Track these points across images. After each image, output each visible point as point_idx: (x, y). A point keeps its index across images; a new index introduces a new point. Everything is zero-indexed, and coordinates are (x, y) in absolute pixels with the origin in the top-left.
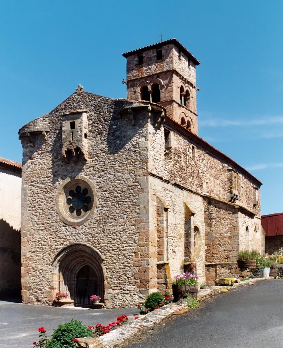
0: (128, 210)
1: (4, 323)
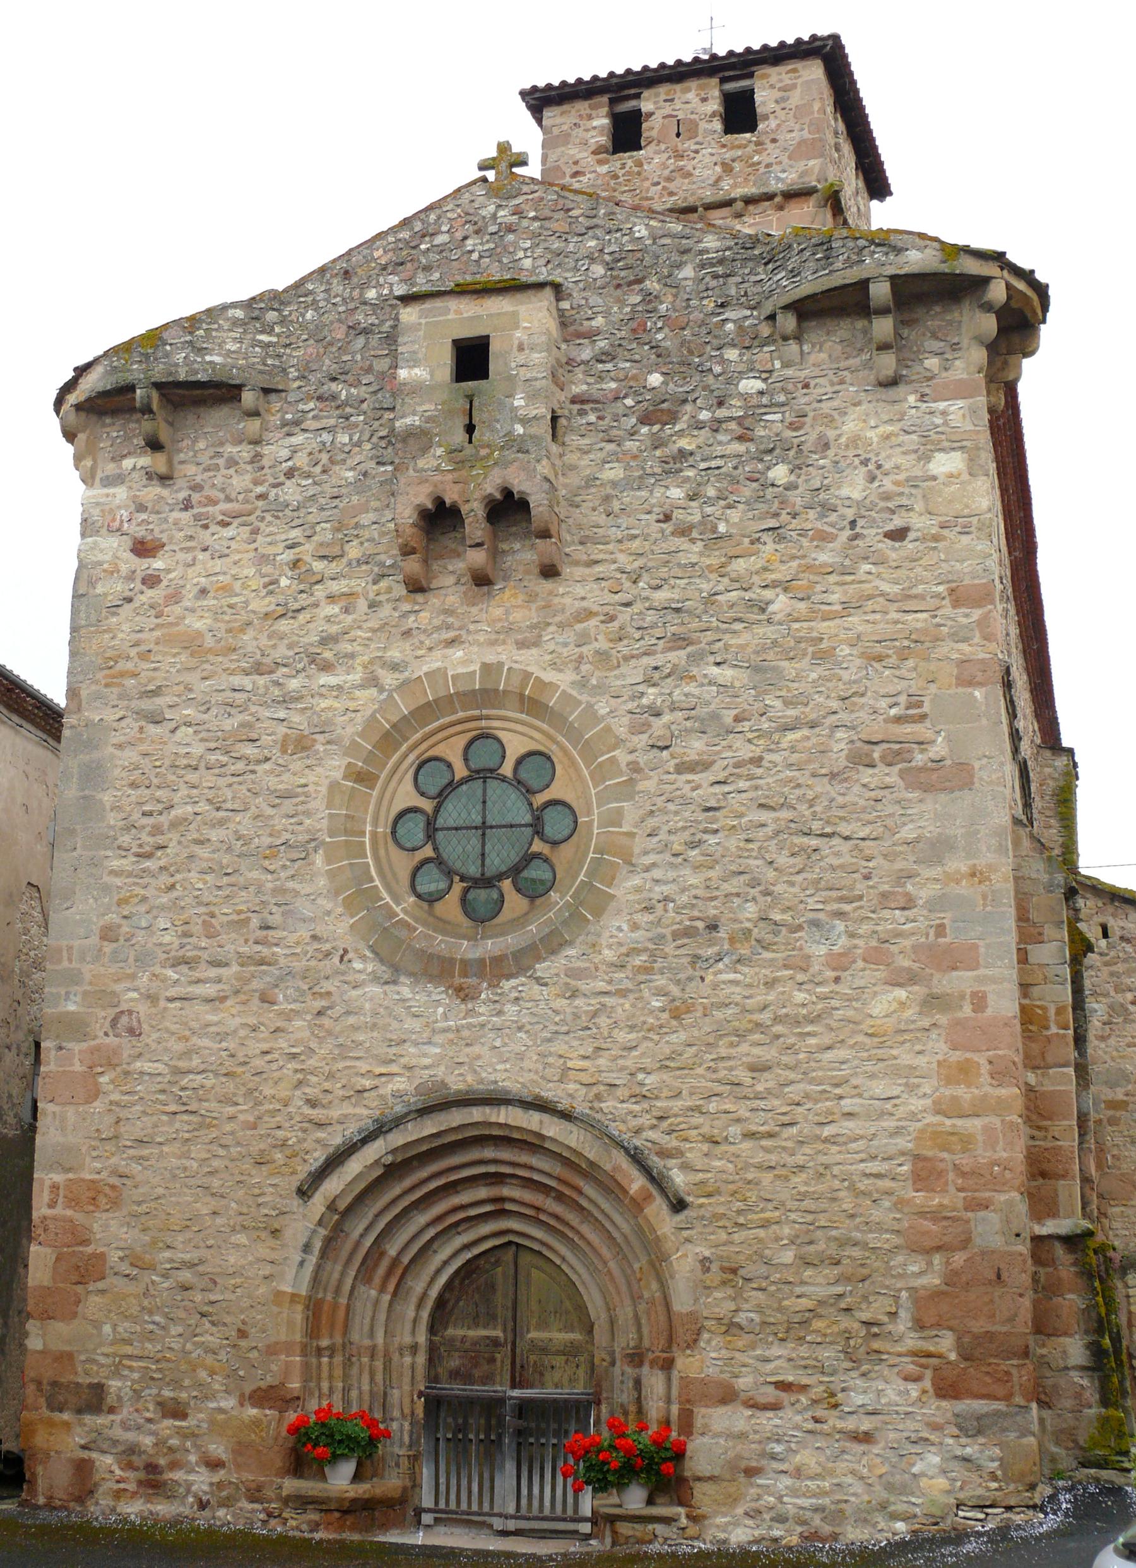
0: (861, 887)
1: (356, 1537)
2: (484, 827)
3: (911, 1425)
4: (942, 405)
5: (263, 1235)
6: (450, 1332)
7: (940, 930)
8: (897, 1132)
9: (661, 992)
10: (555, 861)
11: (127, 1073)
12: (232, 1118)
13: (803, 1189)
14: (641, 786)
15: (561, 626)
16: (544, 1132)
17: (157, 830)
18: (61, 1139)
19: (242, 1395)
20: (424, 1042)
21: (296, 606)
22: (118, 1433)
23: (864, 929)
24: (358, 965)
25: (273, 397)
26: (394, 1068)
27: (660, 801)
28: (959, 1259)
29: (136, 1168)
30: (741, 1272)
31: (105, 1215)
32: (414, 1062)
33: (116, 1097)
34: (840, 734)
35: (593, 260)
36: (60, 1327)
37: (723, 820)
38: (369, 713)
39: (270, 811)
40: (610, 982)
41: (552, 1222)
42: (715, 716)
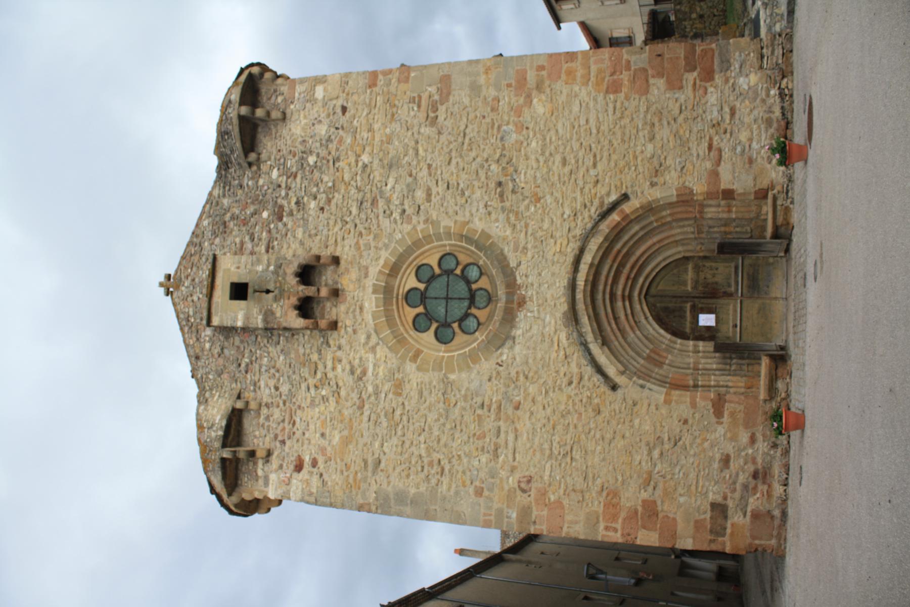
0: (488, 120)
2: (447, 298)
3: (726, 91)
4: (297, 95)
5: (635, 410)
6: (688, 330)
7: (509, 85)
8: (595, 100)
9: (528, 208)
10: (465, 263)
11: (550, 485)
12: (575, 427)
13: (619, 141)
14: (435, 218)
15: (361, 256)
16: (589, 262)
17: (431, 464)
18: (582, 524)
19: (717, 423)
20: (543, 323)
21: (335, 387)
22: (737, 495)
23: (506, 118)
24: (504, 357)
25: (242, 396)
26: (555, 339)
27: (442, 209)
28: (650, 72)
29: (599, 482)
30: (657, 168)
31: (622, 500)
32: (553, 329)
33: (562, 491)
34: (422, 130)
35: (213, 243)
36: (680, 526)
37: (453, 182)
38: (387, 350)
39: (428, 403)
40: (521, 231)
41: (635, 271)
42: (408, 185)
